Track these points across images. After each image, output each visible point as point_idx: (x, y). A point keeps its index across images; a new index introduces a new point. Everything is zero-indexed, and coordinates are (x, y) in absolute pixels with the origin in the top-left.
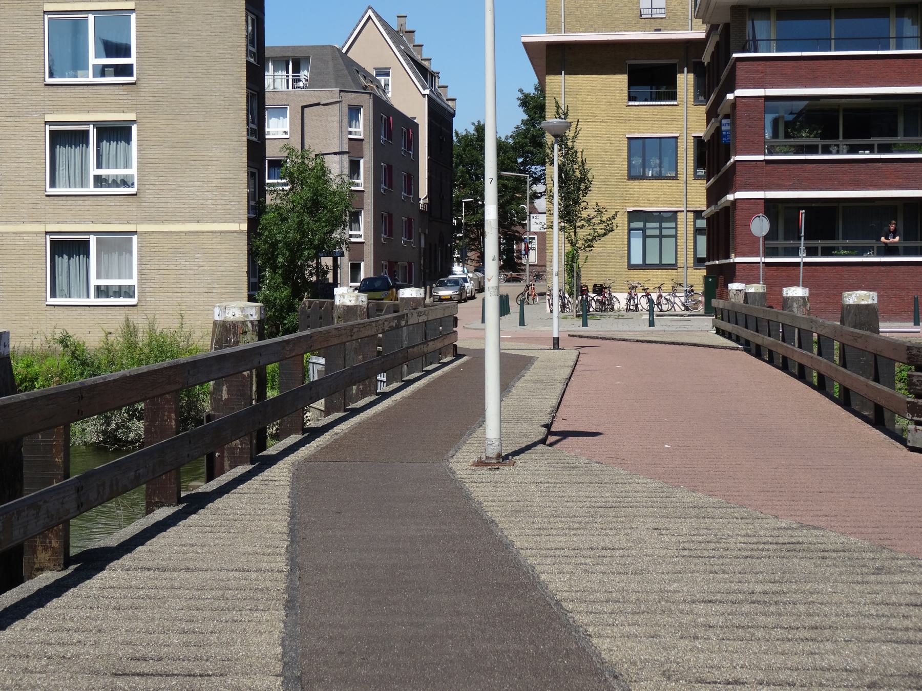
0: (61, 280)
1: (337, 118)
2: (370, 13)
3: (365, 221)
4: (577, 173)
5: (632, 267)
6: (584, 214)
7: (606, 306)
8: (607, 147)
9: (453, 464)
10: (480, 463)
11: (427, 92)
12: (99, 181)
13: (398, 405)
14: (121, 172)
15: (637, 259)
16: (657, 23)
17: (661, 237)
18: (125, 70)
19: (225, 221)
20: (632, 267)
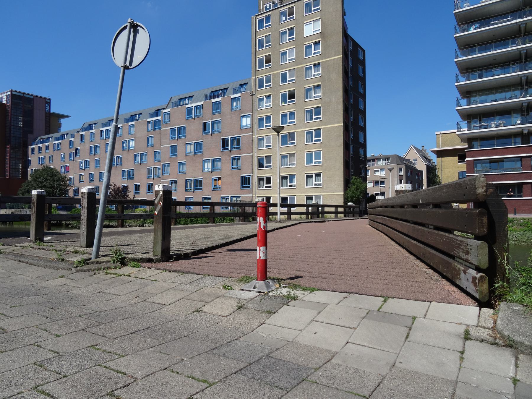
2: (412, 146)
8: (453, 174)
11: (426, 164)
12: (315, 185)
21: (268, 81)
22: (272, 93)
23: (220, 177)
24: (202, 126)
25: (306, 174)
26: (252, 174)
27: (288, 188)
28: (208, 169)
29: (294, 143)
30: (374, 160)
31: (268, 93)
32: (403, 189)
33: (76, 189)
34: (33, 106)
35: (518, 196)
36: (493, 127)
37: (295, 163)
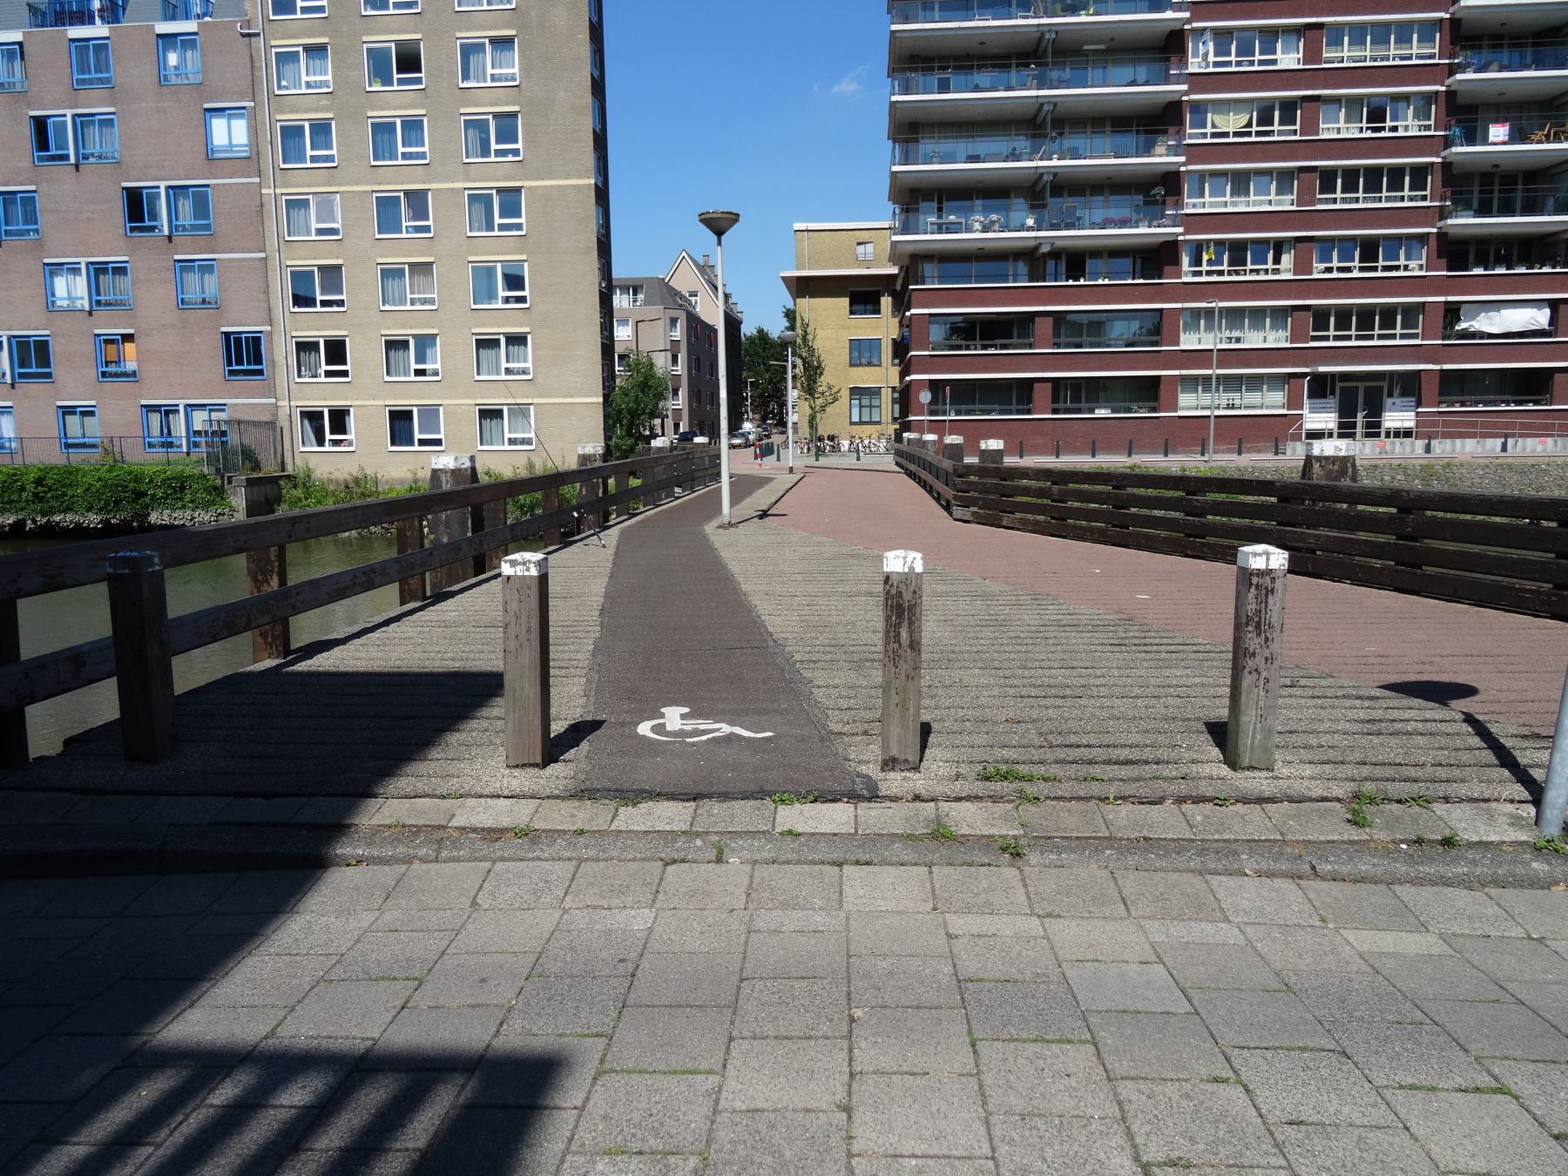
0: (486, 435)
2: (684, 254)
4: (815, 363)
5: (852, 423)
6: (820, 389)
7: (836, 449)
9: (705, 527)
10: (720, 527)
12: (508, 371)
13: (684, 502)
14: (522, 365)
15: (855, 418)
16: (867, 263)
17: (871, 406)
18: (522, 299)
19: (589, 397)
20: (852, 423)
22: (331, 37)
23: (131, 331)
24: (27, 132)
25: (476, 334)
26: (269, 328)
27: (413, 378)
28: (70, 297)
29: (427, 229)
31: (314, 37)
32: (1343, 453)
35: (1019, 412)
36: (977, 230)
37: (435, 296)
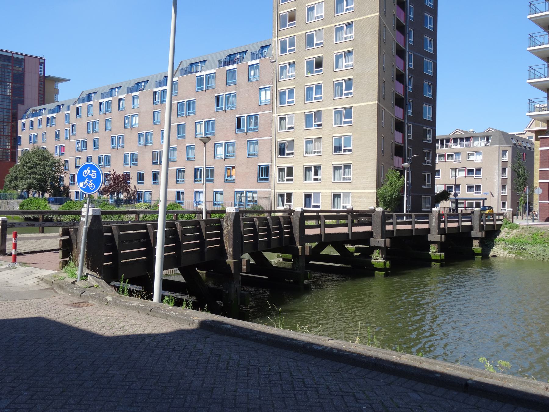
1: (498, 155)
3: (508, 188)
12: (344, 179)
21: (292, 44)
24: (214, 100)
30: (468, 139)
33: (72, 176)
34: (24, 69)
